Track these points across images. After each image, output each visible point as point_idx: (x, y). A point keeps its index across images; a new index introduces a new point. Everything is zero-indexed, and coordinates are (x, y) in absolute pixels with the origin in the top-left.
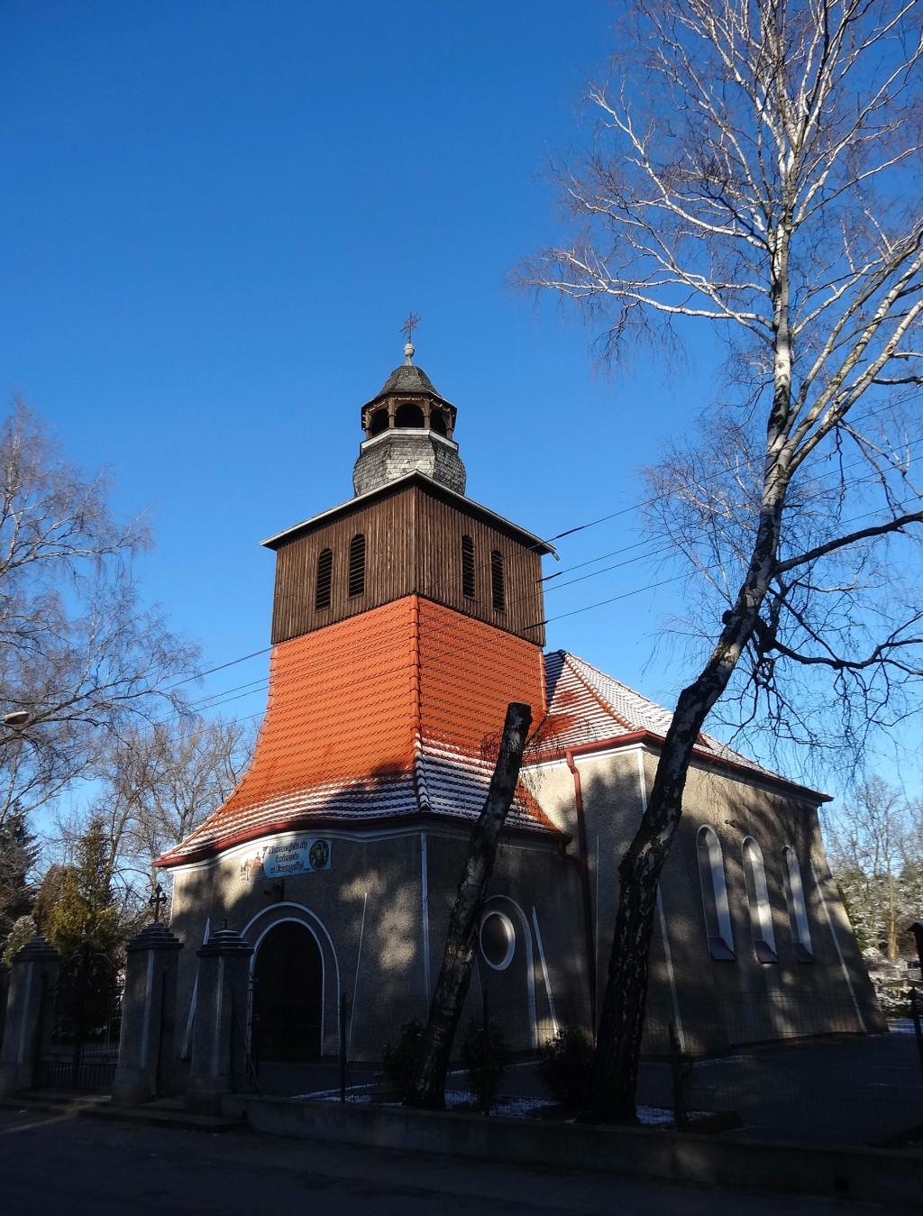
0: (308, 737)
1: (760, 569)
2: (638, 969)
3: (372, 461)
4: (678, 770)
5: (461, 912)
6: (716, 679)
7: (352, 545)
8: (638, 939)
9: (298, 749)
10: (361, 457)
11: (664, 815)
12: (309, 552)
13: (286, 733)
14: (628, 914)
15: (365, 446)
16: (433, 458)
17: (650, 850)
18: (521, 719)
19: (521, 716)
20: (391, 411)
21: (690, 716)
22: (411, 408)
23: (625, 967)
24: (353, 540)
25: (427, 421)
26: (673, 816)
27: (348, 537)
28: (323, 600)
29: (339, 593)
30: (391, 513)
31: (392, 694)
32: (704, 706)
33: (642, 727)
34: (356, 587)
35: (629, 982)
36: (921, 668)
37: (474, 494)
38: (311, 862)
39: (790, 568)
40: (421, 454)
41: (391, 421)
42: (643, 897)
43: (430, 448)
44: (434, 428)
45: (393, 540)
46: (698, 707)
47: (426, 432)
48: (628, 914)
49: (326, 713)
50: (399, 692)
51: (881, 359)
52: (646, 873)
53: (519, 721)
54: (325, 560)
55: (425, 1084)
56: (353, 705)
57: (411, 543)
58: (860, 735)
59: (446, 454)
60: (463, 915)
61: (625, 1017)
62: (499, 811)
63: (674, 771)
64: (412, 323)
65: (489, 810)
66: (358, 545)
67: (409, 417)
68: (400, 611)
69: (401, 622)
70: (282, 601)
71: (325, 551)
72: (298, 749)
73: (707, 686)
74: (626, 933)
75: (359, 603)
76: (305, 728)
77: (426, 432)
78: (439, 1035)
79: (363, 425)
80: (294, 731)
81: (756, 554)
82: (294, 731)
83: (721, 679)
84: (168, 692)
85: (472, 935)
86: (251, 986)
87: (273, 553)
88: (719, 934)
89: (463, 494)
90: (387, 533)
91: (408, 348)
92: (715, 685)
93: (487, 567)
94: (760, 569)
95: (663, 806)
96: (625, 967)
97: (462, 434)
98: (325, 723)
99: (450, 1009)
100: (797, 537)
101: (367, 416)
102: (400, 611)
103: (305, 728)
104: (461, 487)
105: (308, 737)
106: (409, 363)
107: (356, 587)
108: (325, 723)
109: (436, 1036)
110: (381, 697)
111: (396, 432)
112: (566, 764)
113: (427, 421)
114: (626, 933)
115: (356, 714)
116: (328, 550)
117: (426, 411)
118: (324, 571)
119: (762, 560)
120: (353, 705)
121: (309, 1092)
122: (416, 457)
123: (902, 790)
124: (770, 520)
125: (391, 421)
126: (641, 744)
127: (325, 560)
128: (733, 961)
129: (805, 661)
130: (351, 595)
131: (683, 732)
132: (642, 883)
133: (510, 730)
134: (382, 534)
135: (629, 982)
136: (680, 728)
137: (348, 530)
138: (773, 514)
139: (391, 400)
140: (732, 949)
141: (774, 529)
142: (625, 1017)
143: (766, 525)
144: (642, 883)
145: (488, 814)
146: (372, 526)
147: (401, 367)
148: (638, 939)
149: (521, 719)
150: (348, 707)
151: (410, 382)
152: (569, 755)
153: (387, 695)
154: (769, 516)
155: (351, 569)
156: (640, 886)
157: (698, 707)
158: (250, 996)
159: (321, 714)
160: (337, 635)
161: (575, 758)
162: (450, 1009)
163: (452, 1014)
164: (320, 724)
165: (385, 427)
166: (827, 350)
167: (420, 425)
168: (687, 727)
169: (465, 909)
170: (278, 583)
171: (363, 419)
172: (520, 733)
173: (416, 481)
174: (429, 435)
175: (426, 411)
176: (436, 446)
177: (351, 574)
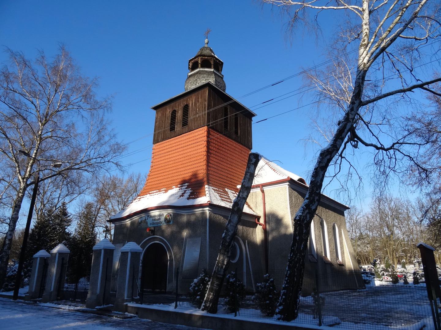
0: (165, 177)
1: (355, 103)
2: (302, 260)
3: (192, 79)
4: (319, 181)
5: (227, 236)
6: (336, 147)
7: (184, 108)
8: (302, 248)
9: (161, 181)
10: (188, 78)
11: (314, 199)
12: (169, 111)
13: (157, 176)
14: (298, 238)
15: (189, 74)
16: (214, 79)
17: (307, 213)
18: (255, 160)
19: (255, 158)
20: (199, 62)
21: (325, 160)
22: (207, 61)
23: (296, 259)
24: (184, 106)
25: (212, 66)
26: (317, 200)
27: (182, 105)
28: (172, 129)
29: (178, 127)
30: (199, 97)
31: (197, 162)
32: (331, 157)
33: (289, 177)
34: (185, 123)
35: (297, 265)
36: (440, 130)
37: (229, 92)
38: (165, 221)
39: (367, 104)
40: (210, 77)
41: (199, 65)
42: (304, 231)
43: (213, 76)
44: (215, 68)
45: (199, 107)
46: (328, 157)
47: (212, 70)
48: (298, 238)
49: (173, 169)
50: (199, 161)
51: (418, 9)
52: (306, 222)
53: (254, 160)
54: (174, 113)
55: (210, 304)
56: (182, 166)
57: (206, 108)
58: (387, 173)
59: (219, 78)
60: (228, 237)
61: (295, 279)
62: (245, 196)
63: (318, 182)
64: (208, 32)
65: (240, 196)
66: (186, 109)
67: (206, 64)
68: (201, 132)
69: (201, 136)
70: (157, 128)
71: (174, 111)
72: (161, 181)
73: (332, 149)
74: (297, 246)
75: (186, 128)
76: (164, 174)
77: (212, 70)
78: (216, 285)
79: (189, 67)
80: (161, 175)
81: (353, 98)
82: (161, 175)
83: (338, 146)
84: (115, 162)
85: (231, 246)
86: (141, 265)
87: (155, 111)
88: (312, 253)
89: (225, 92)
90: (197, 104)
91: (206, 41)
92: (335, 149)
93: (230, 123)
94: (355, 103)
95: (313, 195)
96: (296, 259)
97: (225, 71)
98: (172, 172)
99: (221, 275)
100: (368, 93)
101: (191, 64)
102: (201, 132)
103: (164, 174)
104: (224, 90)
105: (165, 177)
106: (206, 46)
107: (185, 123)
108: (172, 172)
109: (215, 285)
110: (193, 163)
111: (201, 69)
112: (260, 190)
113: (212, 66)
114: (297, 246)
115: (184, 169)
116: (175, 110)
117: (212, 62)
118: (172, 119)
119: (356, 100)
120: (182, 166)
121: (150, 303)
122: (208, 79)
123: (362, 211)
124: (360, 84)
125: (199, 65)
126: (288, 183)
127: (174, 113)
128: (316, 263)
129: (367, 145)
130: (183, 126)
131: (322, 166)
132: (304, 226)
133: (250, 164)
134: (195, 102)
135: (297, 265)
136: (321, 165)
137: (182, 103)
138: (361, 82)
139: (200, 58)
140: (316, 258)
141: (361, 88)
142: (295, 279)
143: (358, 86)
144: (304, 226)
145: (240, 197)
146: (191, 101)
147: (204, 47)
148: (302, 248)
149: (255, 160)
150: (180, 166)
151: (207, 52)
152: (261, 186)
153: (195, 162)
154: (359, 83)
155: (183, 117)
156: (303, 227)
157: (328, 157)
158: (140, 268)
159: (171, 169)
160: (177, 141)
161: (264, 188)
162: (221, 275)
163: (222, 277)
164: (170, 172)
165: (197, 67)
166: (386, 17)
167: (210, 67)
168: (324, 164)
169: (229, 235)
170: (156, 122)
171: (189, 65)
172: (254, 165)
173: (208, 85)
174: (213, 71)
175: (212, 62)
176: (215, 74)
177: (183, 119)
